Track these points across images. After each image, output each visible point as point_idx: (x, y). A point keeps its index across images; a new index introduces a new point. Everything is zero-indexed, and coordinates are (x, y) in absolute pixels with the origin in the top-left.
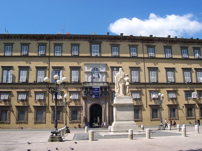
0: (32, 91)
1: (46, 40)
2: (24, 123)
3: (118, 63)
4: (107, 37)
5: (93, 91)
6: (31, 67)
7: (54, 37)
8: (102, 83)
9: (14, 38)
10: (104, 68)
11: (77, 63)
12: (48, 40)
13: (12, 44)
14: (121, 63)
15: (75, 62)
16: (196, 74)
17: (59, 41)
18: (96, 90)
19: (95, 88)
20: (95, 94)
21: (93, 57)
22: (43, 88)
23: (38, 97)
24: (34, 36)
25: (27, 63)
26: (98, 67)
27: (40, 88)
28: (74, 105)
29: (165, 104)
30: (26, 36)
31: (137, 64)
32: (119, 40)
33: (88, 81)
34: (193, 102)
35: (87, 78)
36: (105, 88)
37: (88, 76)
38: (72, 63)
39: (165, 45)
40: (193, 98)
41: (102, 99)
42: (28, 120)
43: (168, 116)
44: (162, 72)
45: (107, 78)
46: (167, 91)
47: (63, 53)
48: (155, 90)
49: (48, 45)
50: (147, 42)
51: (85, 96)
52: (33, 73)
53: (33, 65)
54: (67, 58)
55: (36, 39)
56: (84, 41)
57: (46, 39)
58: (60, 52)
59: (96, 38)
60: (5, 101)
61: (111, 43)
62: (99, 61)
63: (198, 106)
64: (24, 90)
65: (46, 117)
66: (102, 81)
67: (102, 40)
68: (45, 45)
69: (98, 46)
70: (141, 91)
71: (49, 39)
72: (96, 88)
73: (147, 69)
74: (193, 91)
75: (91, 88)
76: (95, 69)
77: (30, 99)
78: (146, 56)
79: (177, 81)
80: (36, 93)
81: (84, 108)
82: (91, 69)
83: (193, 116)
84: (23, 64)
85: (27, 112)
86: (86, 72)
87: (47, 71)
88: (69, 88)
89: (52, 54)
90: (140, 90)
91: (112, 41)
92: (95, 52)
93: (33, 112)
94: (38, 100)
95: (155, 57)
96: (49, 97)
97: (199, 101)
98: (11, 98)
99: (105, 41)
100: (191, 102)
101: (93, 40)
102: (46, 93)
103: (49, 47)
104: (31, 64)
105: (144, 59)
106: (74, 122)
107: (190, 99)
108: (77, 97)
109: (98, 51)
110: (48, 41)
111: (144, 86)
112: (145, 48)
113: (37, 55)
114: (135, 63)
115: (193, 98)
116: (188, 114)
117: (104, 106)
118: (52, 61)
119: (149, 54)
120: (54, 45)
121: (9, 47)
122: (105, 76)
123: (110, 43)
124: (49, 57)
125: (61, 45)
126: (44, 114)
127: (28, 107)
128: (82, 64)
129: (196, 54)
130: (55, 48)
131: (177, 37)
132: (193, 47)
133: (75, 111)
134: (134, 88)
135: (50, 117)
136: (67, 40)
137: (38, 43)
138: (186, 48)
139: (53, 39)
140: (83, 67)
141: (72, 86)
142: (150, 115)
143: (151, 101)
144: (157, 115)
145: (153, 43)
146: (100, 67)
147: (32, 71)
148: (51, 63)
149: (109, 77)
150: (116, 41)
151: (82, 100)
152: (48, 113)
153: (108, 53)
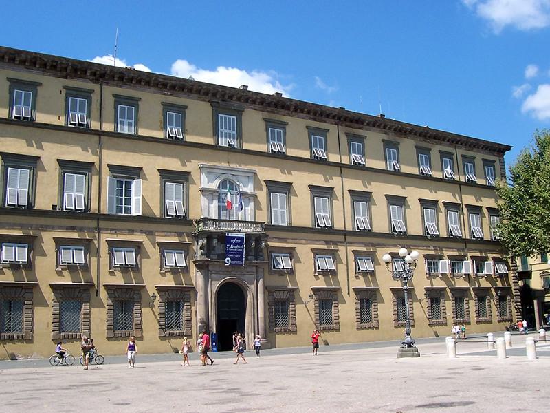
0: (48, 239)
1: (91, 80)
2: (19, 341)
3: (283, 172)
4: (259, 97)
5: (228, 246)
6: (44, 160)
7: (117, 76)
8: (212, 223)
9: (8, 62)
10: (249, 182)
11: (80, 148)
12: (96, 81)
13: (34, 86)
14: (290, 173)
15: (172, 156)
16: (446, 216)
17: (127, 88)
18: (235, 244)
19: (234, 238)
20: (231, 254)
21: (223, 149)
22: (81, 230)
23: (68, 256)
24: (54, 64)
25: (30, 144)
26: (234, 179)
27: (72, 229)
28: (172, 284)
29: (386, 283)
30: (29, 57)
31: (327, 181)
32: (286, 112)
33: (333, 223)
34: (465, 284)
35: (205, 208)
36: (258, 238)
37: (210, 202)
38: (166, 159)
39: (385, 137)
40: (464, 273)
41: (249, 269)
42: (32, 330)
43: (53, 325)
44: (302, 198)
45: (257, 211)
46: (312, 250)
47: (142, 127)
48: (365, 249)
49: (95, 97)
50: (347, 126)
51: (204, 258)
52: (49, 177)
53: (51, 153)
54: (151, 144)
55: (59, 74)
56: (199, 99)
57: (91, 78)
58: (131, 123)
59: (231, 97)
60: (15, 266)
61: (266, 115)
62: (236, 163)
63: (450, 294)
64: (20, 233)
65: (90, 322)
66: (255, 219)
67: (244, 105)
68: (87, 94)
69: (233, 119)
70: (337, 251)
71: (101, 80)
72: (235, 237)
73: (347, 195)
74: (441, 257)
75: (224, 238)
76: (228, 184)
77: (39, 261)
78: (346, 160)
79: (296, 222)
80: (60, 243)
81: (200, 293)
82: (217, 182)
83: (442, 317)
84: (274, 174)
85: (29, 303)
86: (203, 191)
87: (93, 176)
88: (157, 234)
89: (108, 127)
90: (333, 247)
91: (269, 112)
92: (226, 133)
93: (50, 306)
94: (64, 267)
95: (183, 139)
96: (99, 257)
97: (453, 282)
98: (34, 259)
99: (252, 108)
100: (438, 283)
101: (223, 101)
102: (89, 245)
103: (99, 101)
104: (42, 149)
105: (100, 135)
106: (173, 334)
107: (435, 277)
108: (179, 260)
109: (234, 135)
110: (95, 83)
111: (341, 238)
112: (344, 139)
113: (61, 122)
114: (24, 141)
115: (441, 274)
116: (320, 317)
117: (253, 287)
118: (108, 148)
119: (353, 155)
120: (9, 83)
121: (174, 116)
122: (252, 204)
123: (264, 117)
124: (100, 133)
125: (134, 102)
126: (84, 312)
127: (33, 287)
128: (191, 167)
129: (446, 168)
130: (116, 108)
131: (247, 87)
132: (440, 151)
133: (175, 300)
134: (320, 242)
135: (102, 320)
136: (153, 89)
137: (66, 88)
138: (427, 151)
139: (114, 80)
140: (194, 175)
141: (166, 227)
142: (355, 314)
143: (112, 274)
144: (178, 318)
145: (360, 128)
146: (240, 178)
147: (46, 171)
148: (104, 152)
149: (261, 210)
150: (278, 113)
151: (193, 269)
152: (97, 307)
153: (259, 142)
